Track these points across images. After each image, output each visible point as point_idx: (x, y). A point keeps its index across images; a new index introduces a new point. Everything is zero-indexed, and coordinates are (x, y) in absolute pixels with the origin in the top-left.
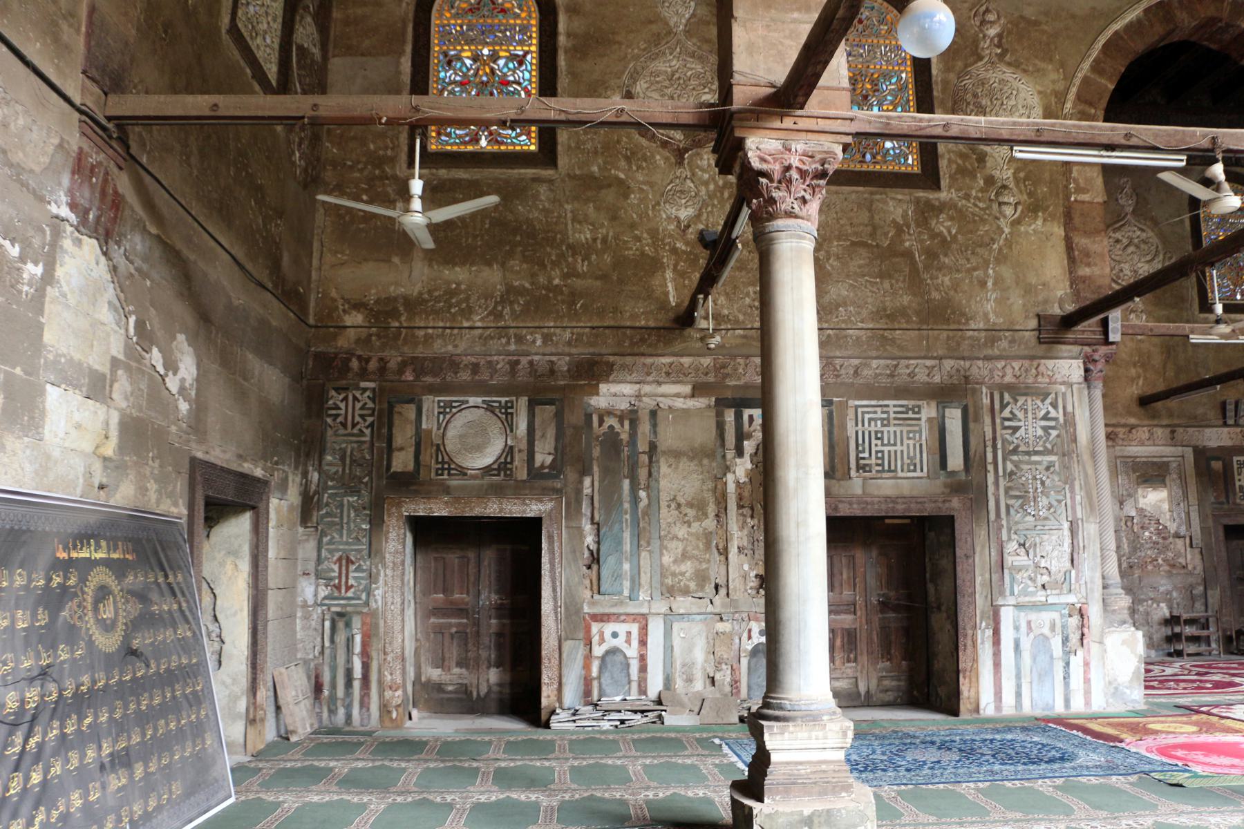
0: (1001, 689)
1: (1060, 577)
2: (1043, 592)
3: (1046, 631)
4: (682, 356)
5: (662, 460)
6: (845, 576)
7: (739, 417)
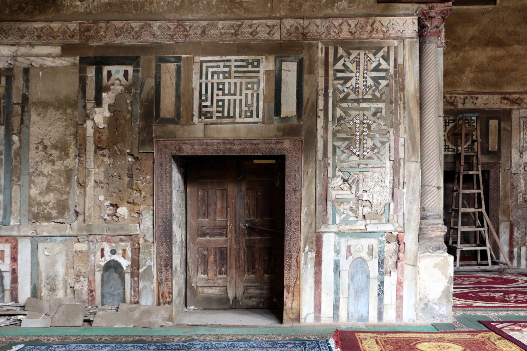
0: (320, 302)
1: (380, 210)
2: (363, 222)
3: (364, 254)
4: (52, 21)
5: (33, 110)
6: (219, 206)
7: (99, 73)
